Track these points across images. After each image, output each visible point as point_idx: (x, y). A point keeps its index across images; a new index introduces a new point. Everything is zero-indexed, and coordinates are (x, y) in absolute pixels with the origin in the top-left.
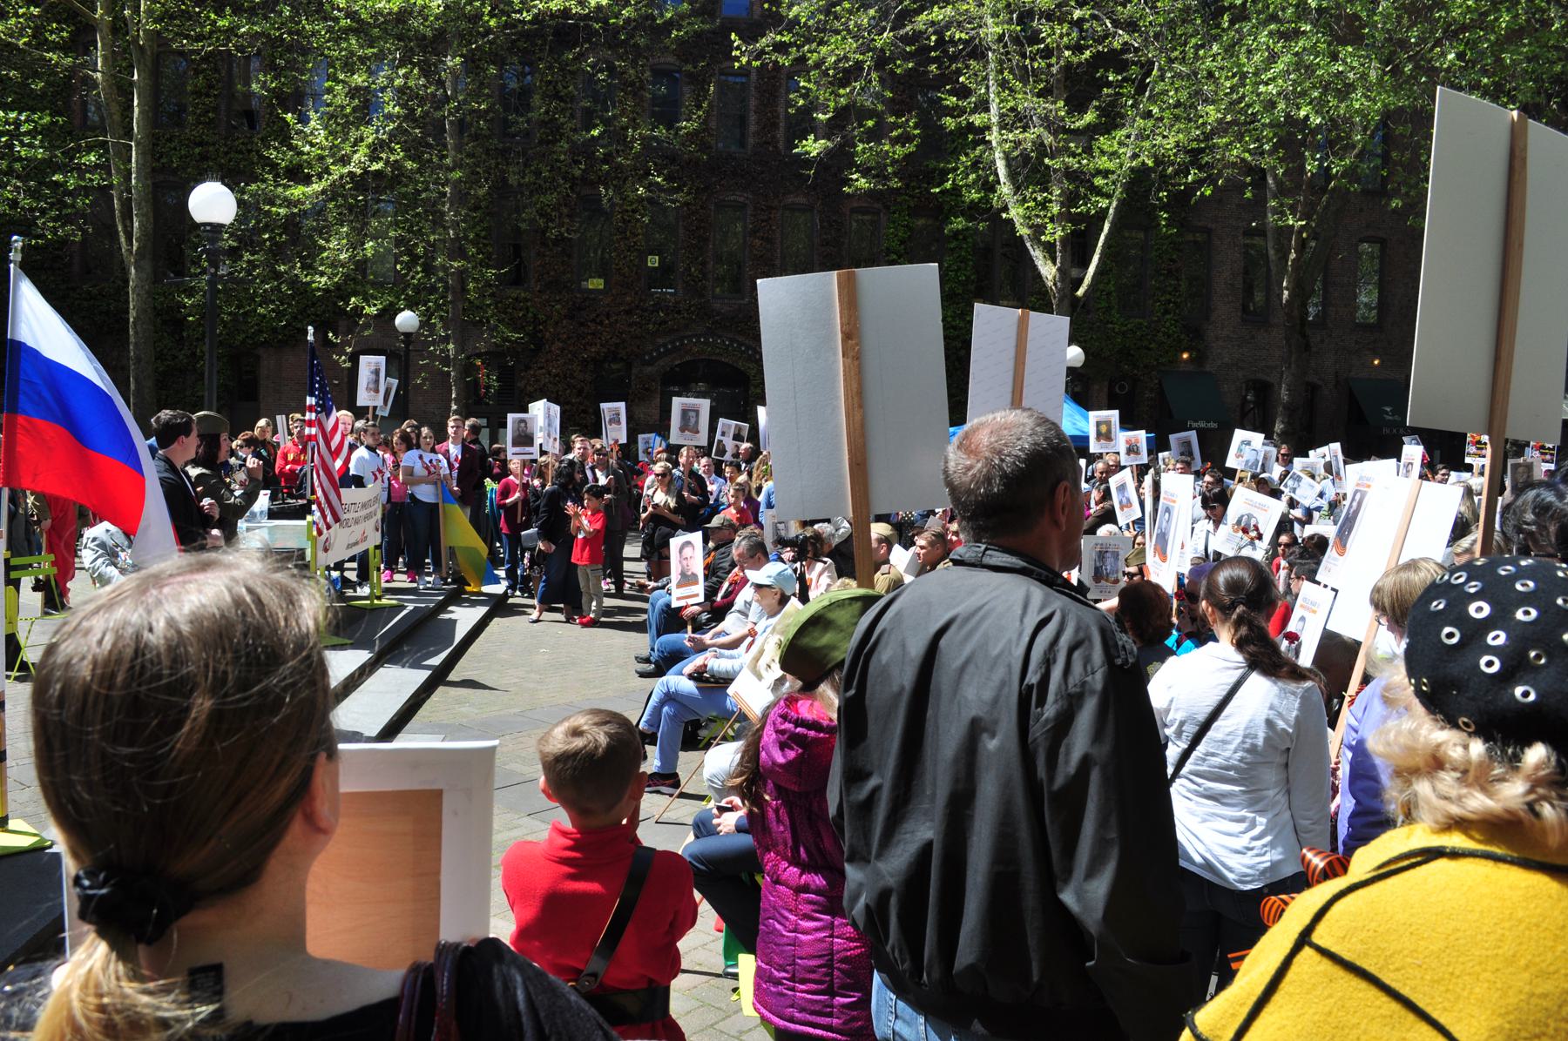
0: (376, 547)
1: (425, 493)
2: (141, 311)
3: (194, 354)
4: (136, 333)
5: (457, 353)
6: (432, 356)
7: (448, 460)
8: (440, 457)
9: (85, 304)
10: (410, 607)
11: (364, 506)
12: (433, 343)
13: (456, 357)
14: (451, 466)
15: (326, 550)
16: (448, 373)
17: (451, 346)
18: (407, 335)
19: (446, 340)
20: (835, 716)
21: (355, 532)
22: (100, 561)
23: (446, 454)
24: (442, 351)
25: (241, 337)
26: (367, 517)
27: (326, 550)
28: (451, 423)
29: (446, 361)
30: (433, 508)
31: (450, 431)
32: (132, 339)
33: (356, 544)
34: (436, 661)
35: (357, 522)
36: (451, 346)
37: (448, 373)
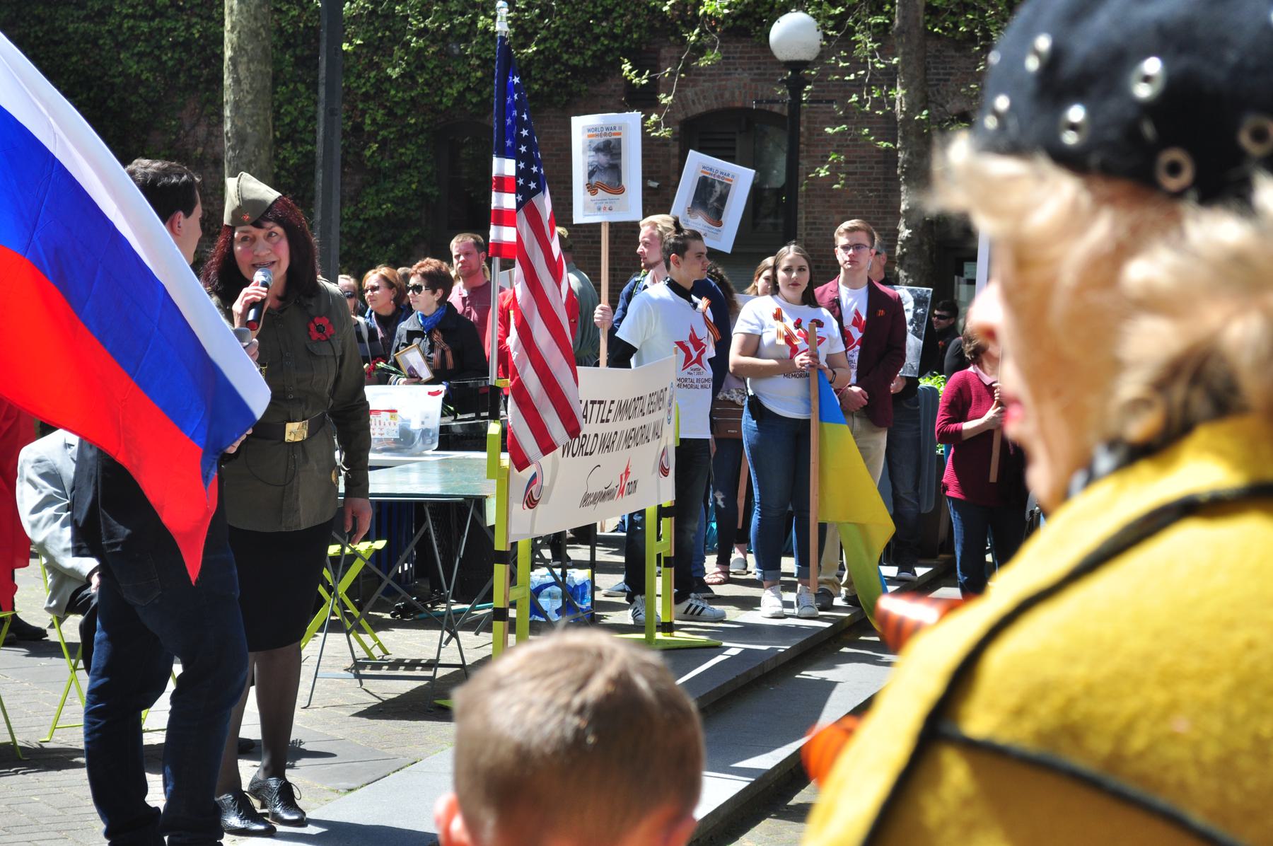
0: (662, 512)
1: (786, 400)
2: (248, 35)
3: (358, 128)
4: (237, 81)
5: (912, 108)
6: (853, 116)
7: (840, 319)
8: (825, 312)
9: (144, 27)
10: (734, 649)
11: (624, 409)
12: (858, 85)
13: (908, 119)
14: (845, 333)
15: (531, 502)
16: (890, 155)
17: (899, 93)
18: (797, 66)
19: (888, 78)
20: (793, 247)
21: (609, 467)
22: (49, 511)
23: (835, 306)
24: (878, 103)
25: (454, 90)
26: (633, 438)
27: (531, 502)
28: (842, 240)
29: (888, 126)
30: (798, 433)
31: (842, 256)
32: (228, 96)
33: (606, 495)
34: (767, 761)
35: (607, 445)
36: (899, 93)
37: (890, 155)
